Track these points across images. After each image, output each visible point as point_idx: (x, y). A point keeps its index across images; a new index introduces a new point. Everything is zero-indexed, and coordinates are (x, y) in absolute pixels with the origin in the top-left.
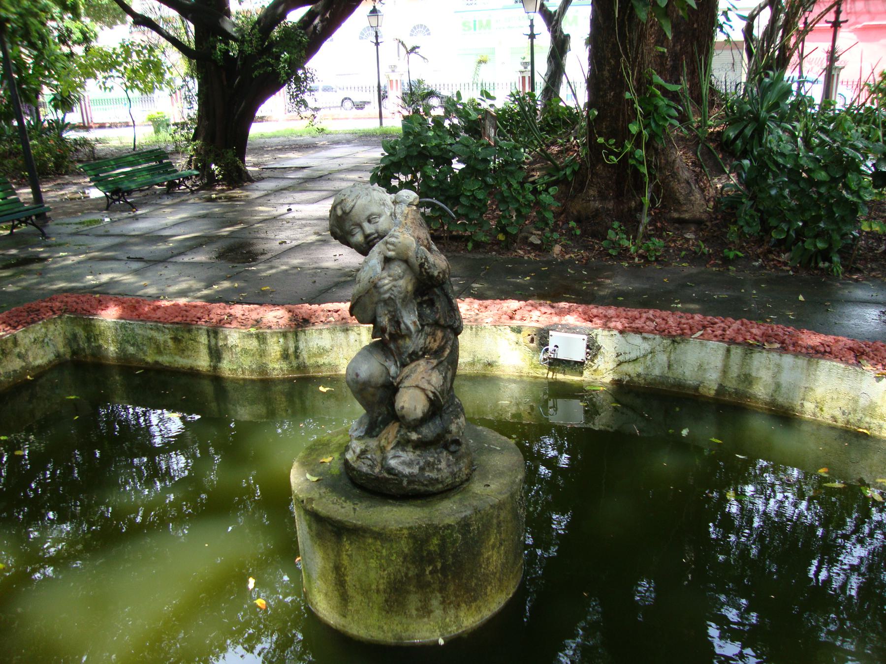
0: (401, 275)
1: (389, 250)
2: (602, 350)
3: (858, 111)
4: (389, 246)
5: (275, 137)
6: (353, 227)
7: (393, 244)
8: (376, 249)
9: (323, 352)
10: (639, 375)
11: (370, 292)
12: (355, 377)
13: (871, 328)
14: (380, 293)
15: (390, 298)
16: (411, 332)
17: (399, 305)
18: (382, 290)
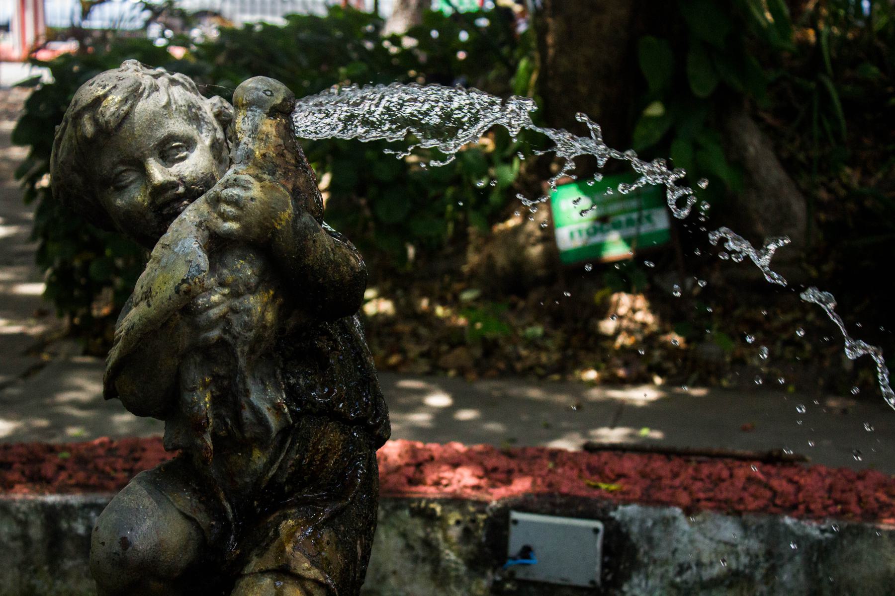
1: (225, 217)
6: (122, 168)
7: (235, 202)
9: (179, 5)
11: (172, 324)
12: (117, 548)
13: (244, 414)
14: (197, 328)
15: (221, 342)
17: (242, 362)
18: (202, 319)
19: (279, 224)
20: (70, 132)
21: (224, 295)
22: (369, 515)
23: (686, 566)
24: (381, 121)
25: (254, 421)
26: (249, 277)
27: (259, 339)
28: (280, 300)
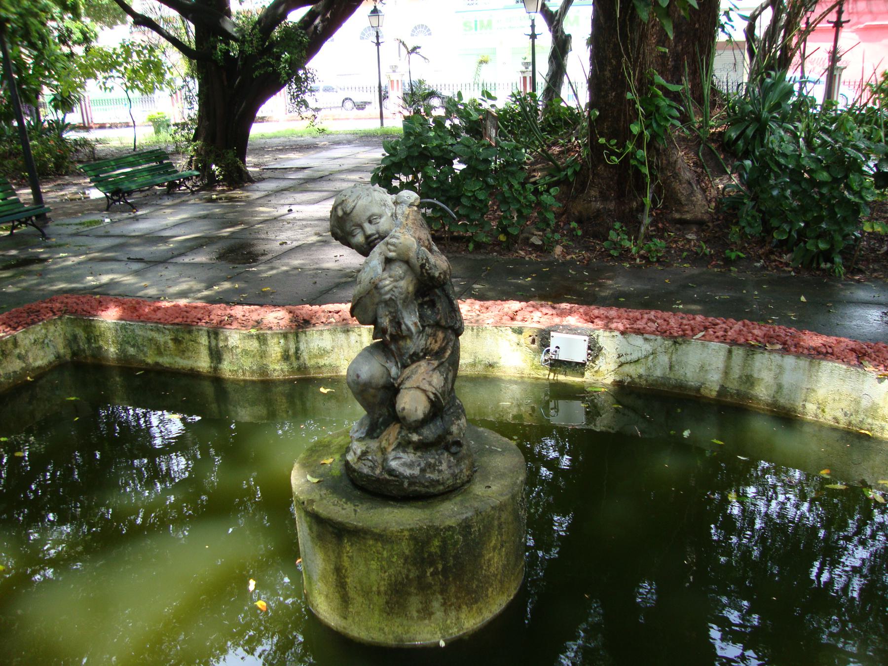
0: (402, 275)
1: (390, 251)
2: (603, 351)
4: (390, 247)
5: (276, 137)
6: (354, 228)
7: (394, 245)
11: (371, 293)
12: (355, 378)
14: (381, 294)
15: (391, 299)
16: (412, 333)
17: (400, 306)
18: (383, 291)
20: (570, 172)
27: (407, 298)
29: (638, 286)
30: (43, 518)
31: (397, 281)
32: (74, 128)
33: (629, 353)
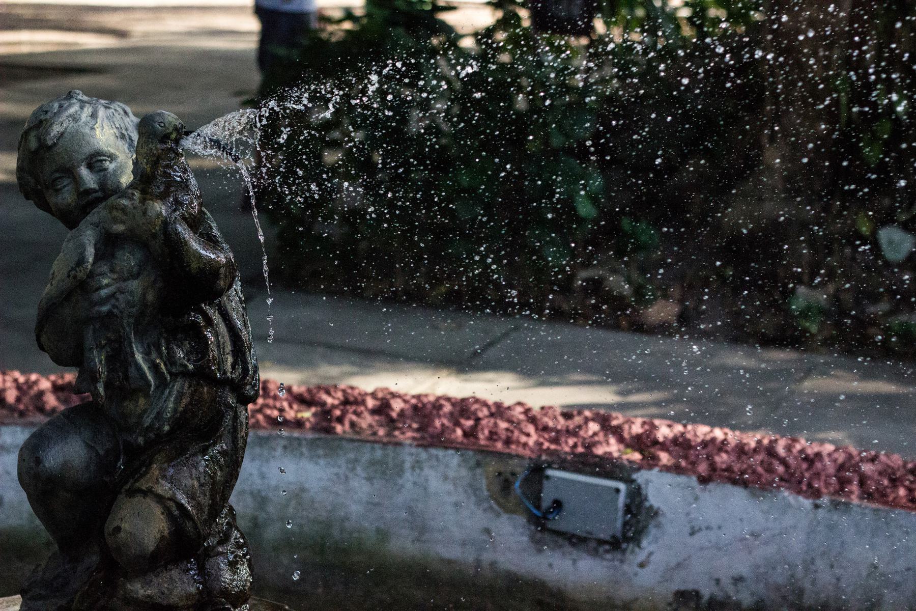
0: (135, 270)
2: (661, 519)
3: (653, 47)
4: (115, 213)
5: (235, 41)
6: (57, 175)
8: (92, 217)
10: (738, 580)
15: (110, 314)
19: (154, 228)
21: (113, 279)
22: (803, 477)
23: (697, 528)
24: (860, 49)
25: (137, 376)
26: (133, 267)
28: (160, 285)
29: (152, 380)
30: (411, 304)
31: (125, 280)
32: (240, 298)
33: (714, 524)
